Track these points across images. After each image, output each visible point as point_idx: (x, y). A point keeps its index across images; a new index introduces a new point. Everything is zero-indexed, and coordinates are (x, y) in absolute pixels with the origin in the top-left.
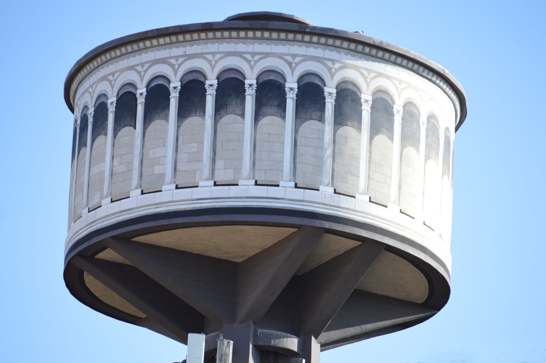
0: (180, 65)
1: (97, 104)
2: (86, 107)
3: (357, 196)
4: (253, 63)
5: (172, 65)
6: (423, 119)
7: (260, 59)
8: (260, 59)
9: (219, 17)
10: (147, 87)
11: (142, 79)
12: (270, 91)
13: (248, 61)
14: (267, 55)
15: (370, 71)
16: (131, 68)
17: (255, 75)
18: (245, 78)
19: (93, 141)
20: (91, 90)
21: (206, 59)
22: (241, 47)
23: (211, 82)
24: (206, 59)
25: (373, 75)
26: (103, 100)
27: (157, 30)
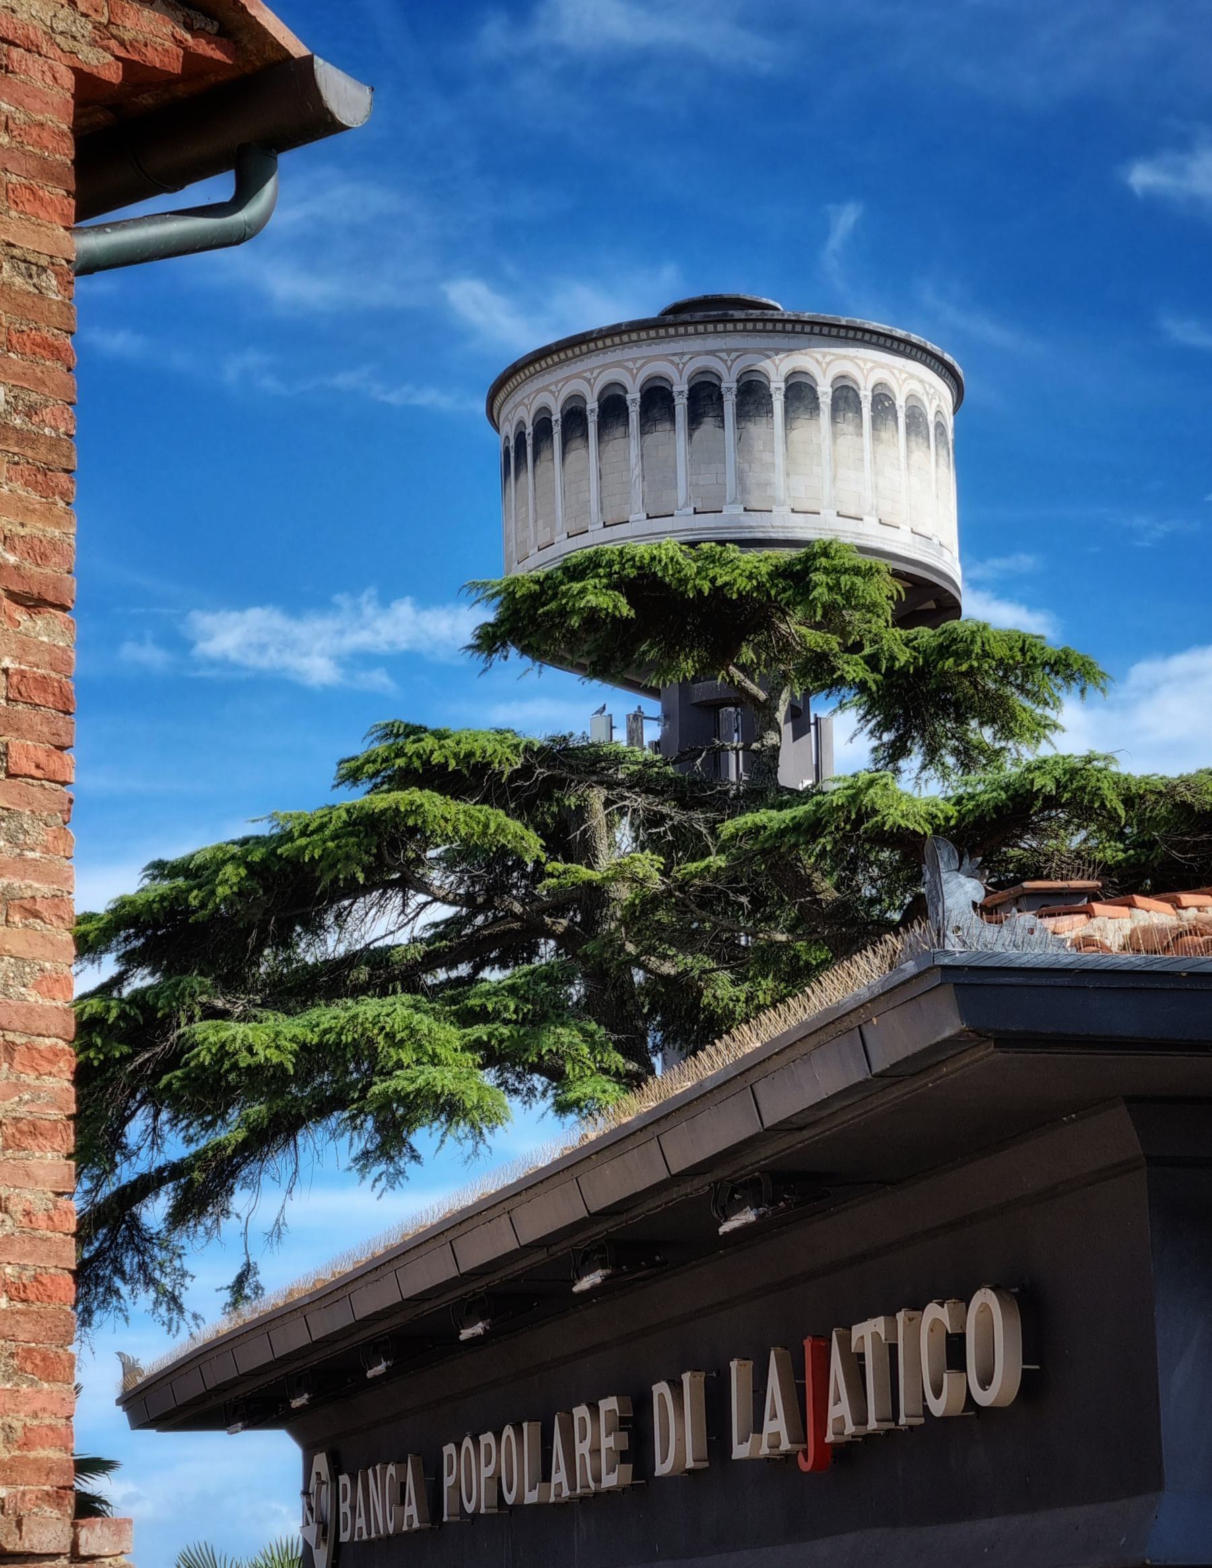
0: (639, 369)
1: (538, 419)
2: (521, 423)
3: (865, 518)
4: (729, 363)
5: (585, 380)
6: (931, 418)
7: (738, 357)
8: (738, 357)
9: (652, 313)
10: (599, 400)
11: (634, 377)
12: (657, 398)
13: (725, 361)
14: (567, 379)
15: (865, 361)
16: (578, 376)
17: (735, 376)
18: (626, 392)
19: (534, 466)
20: (526, 401)
21: (626, 368)
22: (712, 343)
23: (633, 396)
24: (626, 368)
25: (869, 365)
26: (912, 402)
27: (535, 352)
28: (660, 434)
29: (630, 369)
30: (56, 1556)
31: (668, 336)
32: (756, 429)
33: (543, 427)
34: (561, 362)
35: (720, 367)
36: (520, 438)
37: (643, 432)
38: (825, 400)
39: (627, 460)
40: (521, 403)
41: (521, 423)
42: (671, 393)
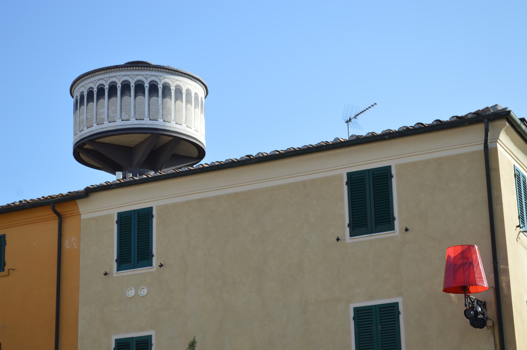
5: (105, 80)
12: (140, 88)
13: (131, 78)
15: (174, 79)
22: (128, 73)
28: (154, 99)
29: (119, 78)
30: (355, 117)
31: (144, 70)
32: (167, 100)
33: (90, 93)
34: (94, 76)
35: (130, 80)
36: (82, 97)
37: (135, 97)
38: (173, 92)
39: (158, 103)
40: (83, 86)
41: (83, 92)
42: (157, 87)
